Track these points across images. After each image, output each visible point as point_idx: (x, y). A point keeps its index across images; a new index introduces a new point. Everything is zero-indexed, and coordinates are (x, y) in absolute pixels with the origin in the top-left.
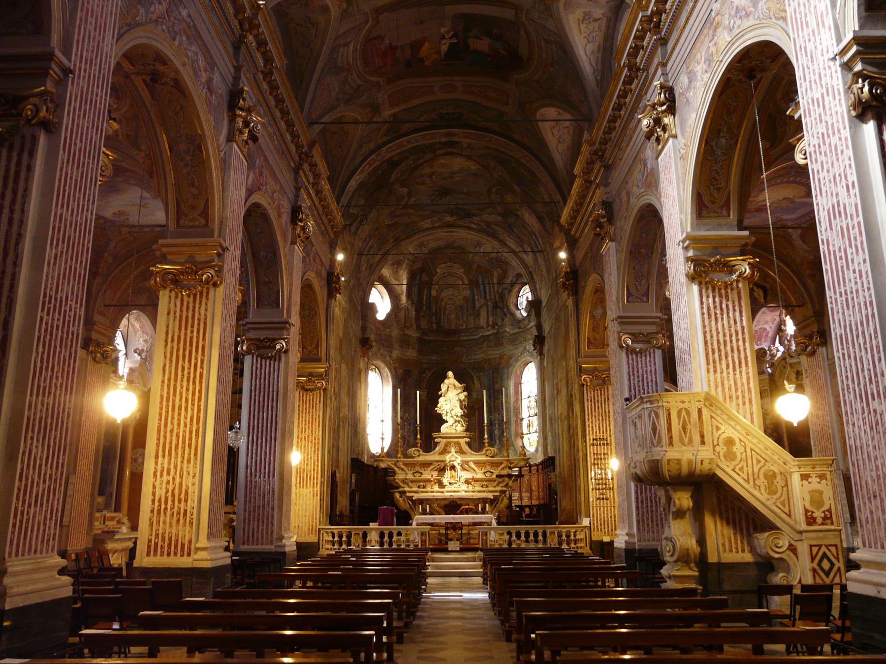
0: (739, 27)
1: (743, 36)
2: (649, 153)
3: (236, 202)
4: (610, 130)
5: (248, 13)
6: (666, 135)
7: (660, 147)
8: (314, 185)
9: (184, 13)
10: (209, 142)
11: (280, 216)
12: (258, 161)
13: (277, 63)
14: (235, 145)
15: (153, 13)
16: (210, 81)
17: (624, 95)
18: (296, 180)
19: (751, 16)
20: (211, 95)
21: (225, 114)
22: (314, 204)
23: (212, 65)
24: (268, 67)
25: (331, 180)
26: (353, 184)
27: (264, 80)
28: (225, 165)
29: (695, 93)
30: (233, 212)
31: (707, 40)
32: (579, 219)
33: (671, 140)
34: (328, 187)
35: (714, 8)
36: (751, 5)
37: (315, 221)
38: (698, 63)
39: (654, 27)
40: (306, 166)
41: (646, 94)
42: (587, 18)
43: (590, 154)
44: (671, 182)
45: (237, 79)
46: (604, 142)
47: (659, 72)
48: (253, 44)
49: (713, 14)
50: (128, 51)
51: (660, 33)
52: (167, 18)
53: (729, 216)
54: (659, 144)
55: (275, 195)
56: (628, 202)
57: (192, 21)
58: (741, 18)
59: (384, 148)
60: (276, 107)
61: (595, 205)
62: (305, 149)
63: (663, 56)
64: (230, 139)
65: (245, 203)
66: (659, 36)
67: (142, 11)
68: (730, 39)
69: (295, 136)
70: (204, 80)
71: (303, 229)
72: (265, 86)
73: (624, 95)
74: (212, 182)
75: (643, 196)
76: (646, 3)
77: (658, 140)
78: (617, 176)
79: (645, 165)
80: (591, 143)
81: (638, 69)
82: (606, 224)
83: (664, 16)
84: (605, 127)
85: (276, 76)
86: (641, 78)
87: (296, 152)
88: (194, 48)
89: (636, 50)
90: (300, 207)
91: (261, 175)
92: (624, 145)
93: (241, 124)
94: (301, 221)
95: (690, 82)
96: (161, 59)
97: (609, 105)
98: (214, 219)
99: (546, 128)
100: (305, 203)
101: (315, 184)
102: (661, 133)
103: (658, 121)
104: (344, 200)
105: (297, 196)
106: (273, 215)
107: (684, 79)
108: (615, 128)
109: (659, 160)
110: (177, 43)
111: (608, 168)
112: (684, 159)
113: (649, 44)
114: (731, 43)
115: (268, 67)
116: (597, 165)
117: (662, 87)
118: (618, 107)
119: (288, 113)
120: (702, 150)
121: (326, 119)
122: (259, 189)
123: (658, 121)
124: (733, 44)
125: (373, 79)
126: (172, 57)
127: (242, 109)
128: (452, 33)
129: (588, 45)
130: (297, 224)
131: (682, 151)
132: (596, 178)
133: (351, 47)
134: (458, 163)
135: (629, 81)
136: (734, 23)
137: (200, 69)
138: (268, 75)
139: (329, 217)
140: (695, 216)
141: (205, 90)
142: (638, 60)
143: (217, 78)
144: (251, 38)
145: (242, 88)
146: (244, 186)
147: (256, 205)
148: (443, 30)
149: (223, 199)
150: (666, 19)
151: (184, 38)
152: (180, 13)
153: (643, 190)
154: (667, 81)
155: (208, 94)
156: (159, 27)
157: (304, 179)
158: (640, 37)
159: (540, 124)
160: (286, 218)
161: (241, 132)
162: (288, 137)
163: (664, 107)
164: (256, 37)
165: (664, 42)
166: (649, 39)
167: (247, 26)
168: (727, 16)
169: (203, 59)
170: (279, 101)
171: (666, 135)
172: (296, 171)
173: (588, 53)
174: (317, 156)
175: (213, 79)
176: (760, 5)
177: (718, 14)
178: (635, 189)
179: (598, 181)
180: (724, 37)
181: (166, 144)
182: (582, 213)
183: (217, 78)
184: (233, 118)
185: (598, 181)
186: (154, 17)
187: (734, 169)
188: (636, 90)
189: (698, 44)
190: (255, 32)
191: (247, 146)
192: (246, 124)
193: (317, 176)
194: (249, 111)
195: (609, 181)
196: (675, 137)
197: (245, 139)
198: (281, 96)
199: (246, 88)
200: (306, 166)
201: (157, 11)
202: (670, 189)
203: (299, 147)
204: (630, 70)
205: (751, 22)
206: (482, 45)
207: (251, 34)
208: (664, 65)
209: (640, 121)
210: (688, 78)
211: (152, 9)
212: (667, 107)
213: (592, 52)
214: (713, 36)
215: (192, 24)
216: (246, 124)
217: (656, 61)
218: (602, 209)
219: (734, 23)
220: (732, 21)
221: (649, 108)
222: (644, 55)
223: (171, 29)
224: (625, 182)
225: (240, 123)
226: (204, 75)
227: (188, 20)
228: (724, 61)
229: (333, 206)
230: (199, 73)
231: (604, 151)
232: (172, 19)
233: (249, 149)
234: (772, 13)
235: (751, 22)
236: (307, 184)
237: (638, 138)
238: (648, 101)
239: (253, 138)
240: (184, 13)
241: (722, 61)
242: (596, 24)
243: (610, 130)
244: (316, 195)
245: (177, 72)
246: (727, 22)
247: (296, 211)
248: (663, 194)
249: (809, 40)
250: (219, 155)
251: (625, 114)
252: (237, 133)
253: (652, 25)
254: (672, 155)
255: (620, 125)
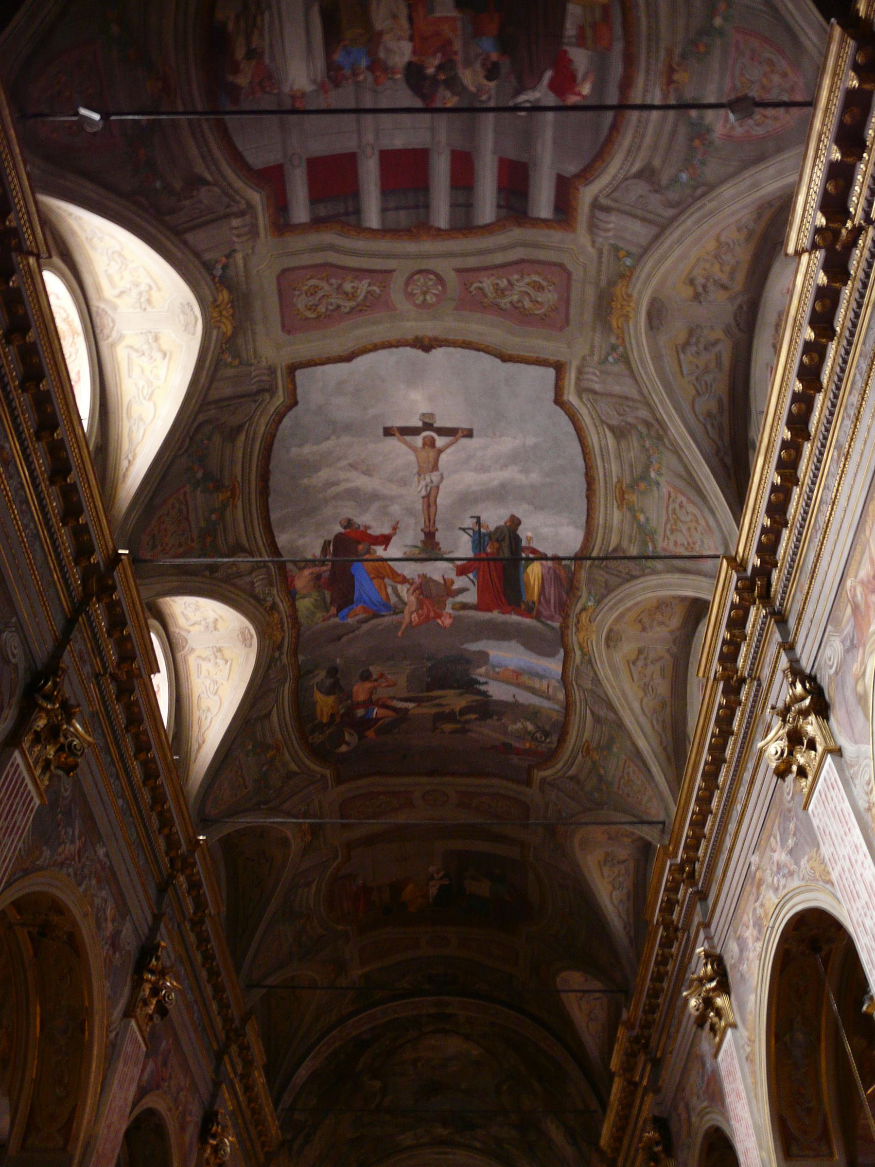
0: (785, 887)
1: (791, 898)
2: (705, 1046)
3: (117, 1110)
4: (652, 1009)
5: (184, 848)
6: (723, 1023)
7: (717, 1039)
8: (243, 1077)
9: (101, 852)
10: (97, 1018)
11: (183, 1128)
12: (164, 1043)
13: (212, 909)
14: (133, 1023)
15: (60, 855)
16: (117, 933)
17: (663, 961)
18: (217, 1070)
19: (795, 876)
20: (114, 953)
21: (129, 979)
22: (240, 1107)
23: (123, 911)
24: (199, 914)
25: (269, 1070)
26: (303, 1073)
27: (192, 930)
28: (112, 1051)
29: (749, 967)
30: (109, 1127)
31: (752, 898)
32: (626, 1143)
33: (729, 1032)
34: (263, 1080)
35: (752, 860)
36: (792, 862)
37: (238, 1136)
38: (748, 927)
39: (688, 877)
40: (234, 1049)
41: (690, 962)
42: (608, 859)
43: (629, 1042)
44: (738, 1095)
45: (154, 930)
46: (647, 1025)
47: (702, 936)
48: (184, 886)
49: (753, 868)
50: (18, 899)
51: (696, 884)
52: (77, 859)
53: (831, 1155)
54: (715, 1035)
55: (182, 1095)
56: (689, 1120)
57: (110, 862)
58: (784, 876)
59: (351, 1021)
60: (203, 965)
61: (645, 1122)
62: (237, 1023)
63: (704, 915)
64: (128, 1013)
65: (131, 1113)
66: (695, 889)
67: (47, 853)
68: (777, 901)
69: (224, 1006)
70: (108, 933)
71: (216, 1149)
72: (192, 938)
73: (663, 961)
74: (88, 1078)
75: (708, 1113)
76: (674, 849)
77: (713, 1028)
78: (670, 1076)
79: (703, 1065)
80: (630, 1026)
81: (676, 929)
82: (663, 1156)
83: (697, 865)
84: (645, 1005)
85: (208, 926)
86: (682, 940)
87: (223, 1028)
88: (104, 893)
89: (669, 906)
90: (216, 1113)
91: (165, 1063)
92: (673, 1030)
93: (147, 992)
94: (214, 1136)
95: (741, 951)
96: (57, 907)
97: (646, 975)
98: (77, 1139)
99: (571, 1001)
100: (226, 1105)
101: (245, 1077)
102: (716, 1020)
103: (708, 1003)
104: (287, 1100)
105: (214, 1095)
106: (172, 1126)
107: (733, 947)
108: (658, 1005)
109: (720, 1058)
110: (82, 889)
111: (657, 1064)
112: (751, 1061)
113: (685, 897)
114: (780, 906)
115: (199, 914)
116: (642, 1058)
117: (707, 955)
118: (659, 977)
119: (218, 974)
120: (773, 1049)
121: (270, 981)
122: (158, 1087)
123: (708, 1003)
124: (783, 906)
125: (340, 927)
126: (71, 906)
127: (152, 972)
128: (442, 873)
129: (614, 893)
130: (207, 1143)
131: (748, 1049)
132: (642, 1078)
133: (314, 887)
134: (453, 1045)
135: (667, 943)
136: (778, 881)
137: (106, 920)
138: (197, 923)
139: (260, 1127)
140: (781, 1155)
141: (107, 947)
142: (675, 917)
143: (127, 931)
144: (182, 878)
145: (158, 945)
146: (135, 1084)
147: (151, 1113)
148: (432, 869)
149: (99, 1104)
150: (701, 869)
151: (94, 882)
152: (95, 852)
153: (705, 1104)
154: (712, 947)
155: (111, 952)
156: (64, 871)
157: (229, 1067)
158: (673, 889)
159: (563, 995)
160: (192, 1131)
161: (146, 1003)
162: (215, 1006)
163: (714, 984)
164: (189, 878)
165: (702, 896)
166: (684, 893)
167: (179, 864)
168: (768, 871)
169: (114, 906)
170: (208, 957)
171: (723, 1023)
172: (219, 1057)
173: (616, 902)
174: (252, 1035)
175: (122, 931)
176: (802, 863)
177: (758, 869)
178: (694, 1101)
179: (645, 1082)
180: (770, 899)
181: (38, 1020)
182: (630, 1128)
183: (127, 931)
184: (138, 983)
185: (645, 1082)
186: (59, 859)
187: (824, 1079)
188: (678, 954)
189: (742, 903)
190: (188, 872)
191: (150, 1024)
192: (155, 991)
193: (248, 1063)
194: (162, 973)
195: (660, 1083)
196: (734, 1026)
197: (150, 1012)
198: (211, 951)
199: (163, 944)
200: (234, 1049)
201: (66, 852)
202: (739, 1106)
203: (227, 1020)
204: (666, 929)
205: (795, 883)
206: (483, 888)
207: (182, 874)
208: (707, 926)
209: (686, 1001)
210: (739, 945)
211: (60, 850)
212: (718, 982)
213: (621, 901)
214: (758, 895)
215: (108, 863)
216: (155, 991)
217: (697, 919)
218: (654, 1129)
219: (778, 881)
220: (776, 879)
221: (695, 983)
222: (681, 910)
223: (79, 872)
224: (680, 1088)
225: (147, 989)
226: (110, 926)
227: (105, 860)
228: (776, 927)
229: (268, 1109)
230: (104, 925)
231: (648, 1039)
232: (83, 860)
233: (153, 1028)
234: (817, 875)
235: (795, 883)
236: (232, 1076)
237: (688, 1026)
238: (693, 973)
239: (162, 1010)
240: (101, 852)
241: (773, 928)
242: (622, 867)
243: (652, 1009)
244: (245, 1093)
245: (74, 923)
246: (770, 880)
247: (209, 1118)
248: (732, 1114)
249: (865, 915)
250: (107, 1036)
251: (668, 987)
252: (140, 1005)
253: (685, 875)
254: (735, 1054)
255: (664, 1002)
